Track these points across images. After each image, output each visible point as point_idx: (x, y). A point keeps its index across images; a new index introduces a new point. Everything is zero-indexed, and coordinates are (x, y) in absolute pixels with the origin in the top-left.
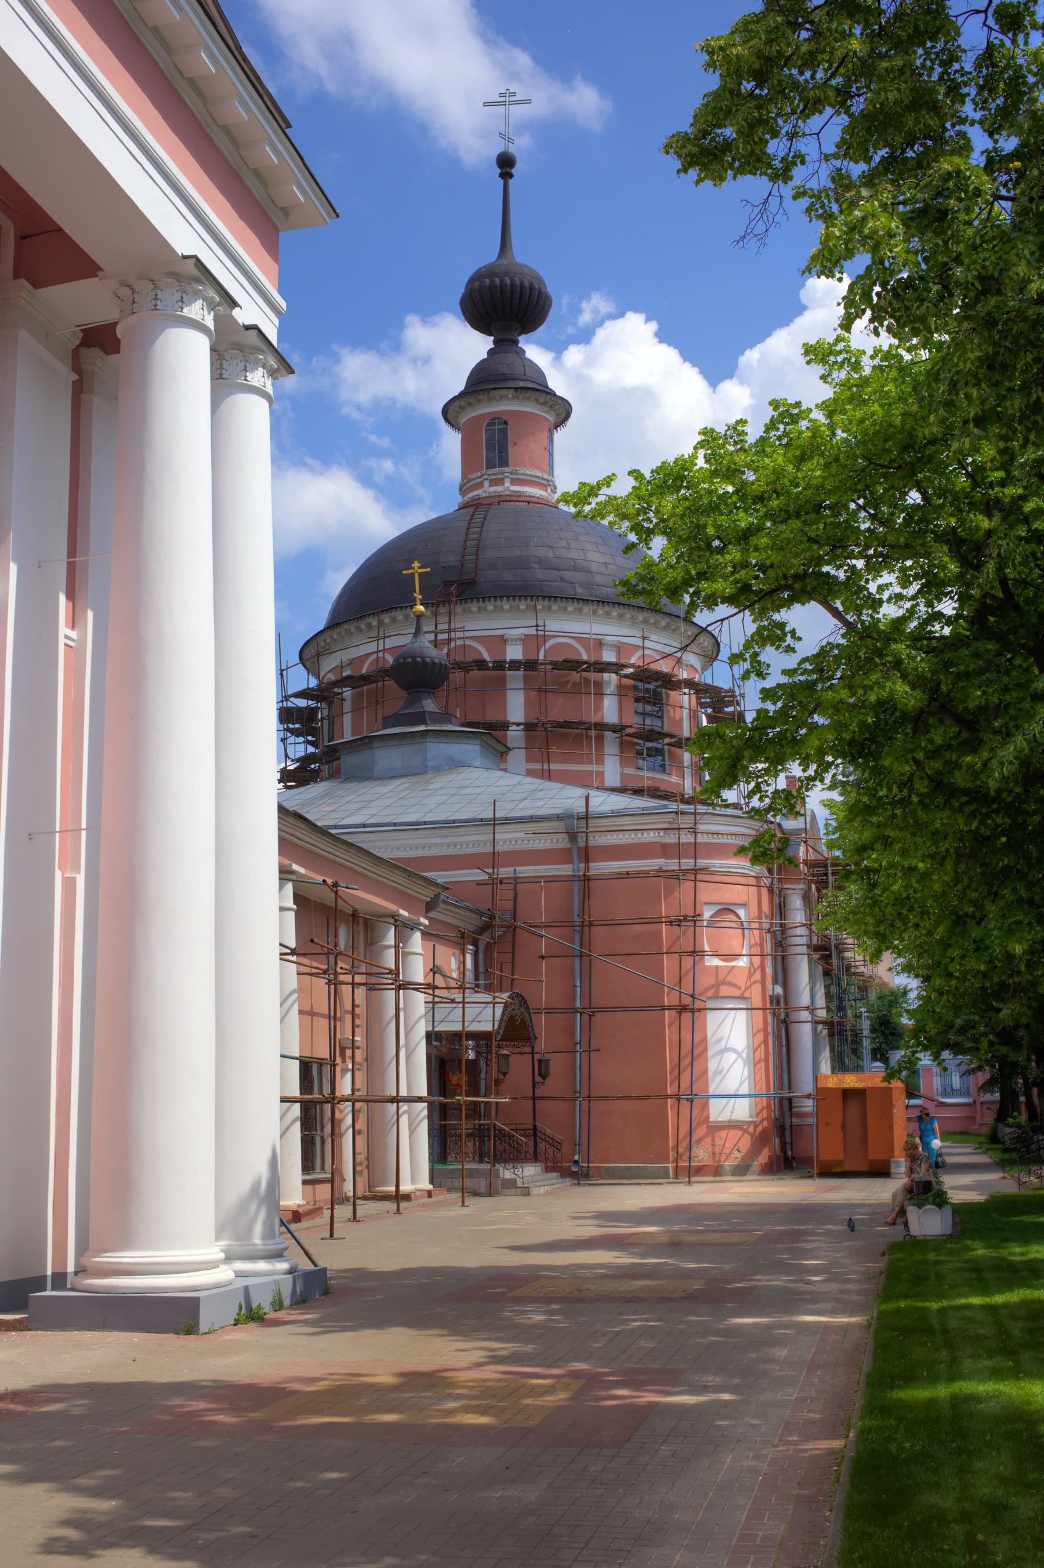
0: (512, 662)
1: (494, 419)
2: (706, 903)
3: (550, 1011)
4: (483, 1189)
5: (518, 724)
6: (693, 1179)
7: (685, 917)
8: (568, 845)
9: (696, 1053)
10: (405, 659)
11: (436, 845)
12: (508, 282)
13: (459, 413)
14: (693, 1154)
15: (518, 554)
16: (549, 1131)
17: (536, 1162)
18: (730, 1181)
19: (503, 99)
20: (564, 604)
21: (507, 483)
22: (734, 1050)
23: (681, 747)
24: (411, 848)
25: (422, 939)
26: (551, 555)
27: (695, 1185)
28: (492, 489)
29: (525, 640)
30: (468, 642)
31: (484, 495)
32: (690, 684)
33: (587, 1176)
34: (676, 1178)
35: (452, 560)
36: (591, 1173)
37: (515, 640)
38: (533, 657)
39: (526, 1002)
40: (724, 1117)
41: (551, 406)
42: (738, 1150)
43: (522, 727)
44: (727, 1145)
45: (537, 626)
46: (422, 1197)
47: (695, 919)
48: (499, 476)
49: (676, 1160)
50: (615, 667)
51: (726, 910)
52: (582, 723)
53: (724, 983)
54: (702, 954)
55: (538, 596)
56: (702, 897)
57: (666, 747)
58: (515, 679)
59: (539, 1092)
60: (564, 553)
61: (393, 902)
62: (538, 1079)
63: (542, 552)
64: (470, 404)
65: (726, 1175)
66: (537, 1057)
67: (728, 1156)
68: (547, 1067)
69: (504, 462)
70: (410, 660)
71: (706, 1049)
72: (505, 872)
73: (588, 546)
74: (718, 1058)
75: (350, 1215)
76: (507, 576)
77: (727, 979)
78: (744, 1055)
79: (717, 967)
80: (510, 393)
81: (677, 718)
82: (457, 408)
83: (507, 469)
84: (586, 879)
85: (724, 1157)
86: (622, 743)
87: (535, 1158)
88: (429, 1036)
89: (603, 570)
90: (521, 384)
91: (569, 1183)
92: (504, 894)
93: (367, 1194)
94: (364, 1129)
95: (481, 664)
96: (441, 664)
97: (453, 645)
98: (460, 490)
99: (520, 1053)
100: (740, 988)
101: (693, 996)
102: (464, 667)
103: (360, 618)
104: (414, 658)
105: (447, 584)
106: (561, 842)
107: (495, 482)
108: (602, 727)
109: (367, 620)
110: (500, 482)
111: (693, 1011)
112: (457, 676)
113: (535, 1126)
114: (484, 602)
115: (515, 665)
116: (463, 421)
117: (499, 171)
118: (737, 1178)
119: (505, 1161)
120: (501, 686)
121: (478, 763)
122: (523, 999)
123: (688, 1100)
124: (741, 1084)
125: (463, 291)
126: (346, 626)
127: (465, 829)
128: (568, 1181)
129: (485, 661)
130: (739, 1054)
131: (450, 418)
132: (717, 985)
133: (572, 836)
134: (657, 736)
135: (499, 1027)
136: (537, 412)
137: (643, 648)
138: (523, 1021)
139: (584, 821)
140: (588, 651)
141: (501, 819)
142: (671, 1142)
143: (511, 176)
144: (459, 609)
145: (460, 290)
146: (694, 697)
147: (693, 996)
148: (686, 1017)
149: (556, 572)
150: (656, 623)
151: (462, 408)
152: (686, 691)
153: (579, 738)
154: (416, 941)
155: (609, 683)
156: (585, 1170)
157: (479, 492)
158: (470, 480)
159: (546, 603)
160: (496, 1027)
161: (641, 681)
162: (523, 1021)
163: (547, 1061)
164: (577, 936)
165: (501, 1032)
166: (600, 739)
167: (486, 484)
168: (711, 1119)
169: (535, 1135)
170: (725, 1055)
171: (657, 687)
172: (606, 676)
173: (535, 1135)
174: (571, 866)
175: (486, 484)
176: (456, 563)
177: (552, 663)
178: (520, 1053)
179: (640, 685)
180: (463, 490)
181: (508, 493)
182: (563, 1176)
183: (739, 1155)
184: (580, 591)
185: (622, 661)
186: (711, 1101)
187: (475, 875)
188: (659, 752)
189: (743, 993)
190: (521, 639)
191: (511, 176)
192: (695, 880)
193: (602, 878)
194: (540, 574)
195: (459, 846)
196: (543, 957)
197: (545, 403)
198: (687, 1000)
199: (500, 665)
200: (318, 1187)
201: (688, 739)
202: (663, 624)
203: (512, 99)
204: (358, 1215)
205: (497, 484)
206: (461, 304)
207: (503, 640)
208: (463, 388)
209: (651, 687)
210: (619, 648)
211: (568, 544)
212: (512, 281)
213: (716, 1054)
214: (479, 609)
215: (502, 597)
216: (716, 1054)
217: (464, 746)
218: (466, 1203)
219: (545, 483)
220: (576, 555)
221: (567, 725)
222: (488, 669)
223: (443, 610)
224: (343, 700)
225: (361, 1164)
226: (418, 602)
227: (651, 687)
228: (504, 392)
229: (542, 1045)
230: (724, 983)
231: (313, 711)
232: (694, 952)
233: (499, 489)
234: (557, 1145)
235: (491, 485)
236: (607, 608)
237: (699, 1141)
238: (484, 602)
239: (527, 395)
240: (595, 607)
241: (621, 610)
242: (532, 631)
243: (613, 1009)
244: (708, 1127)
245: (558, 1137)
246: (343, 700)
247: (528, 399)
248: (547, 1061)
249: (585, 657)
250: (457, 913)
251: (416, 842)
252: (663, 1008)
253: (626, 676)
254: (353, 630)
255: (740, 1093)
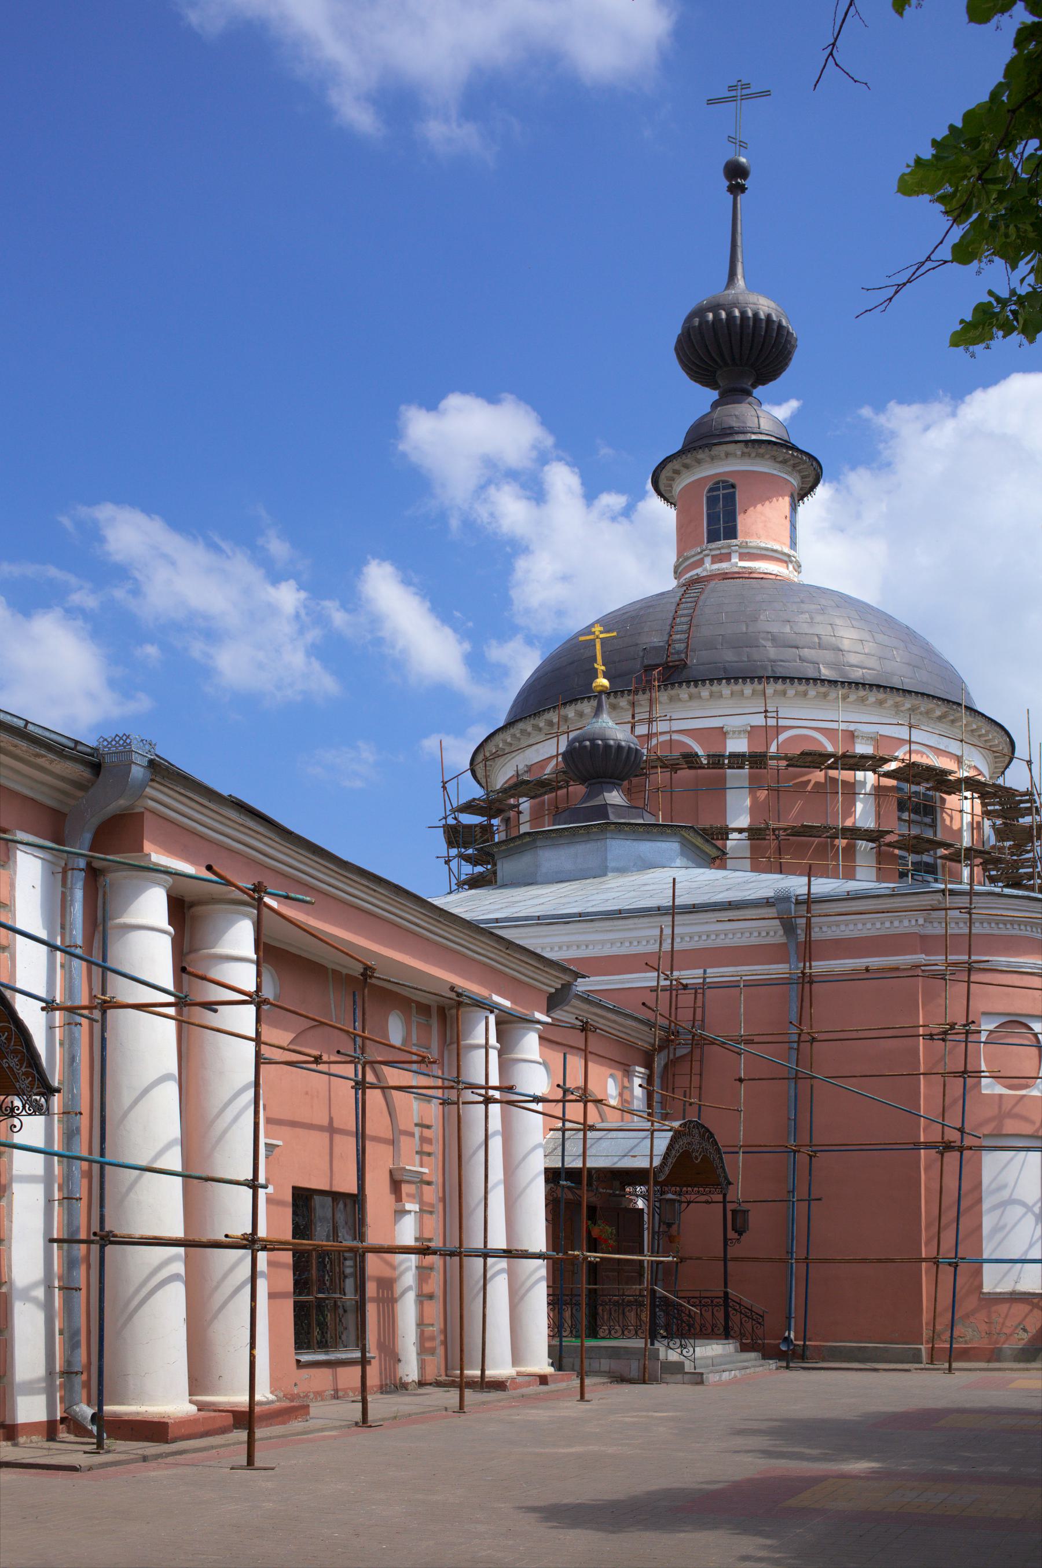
0: (733, 756)
1: (718, 483)
2: (984, 1014)
3: (751, 1150)
4: (634, 1374)
5: (740, 831)
6: (955, 1365)
7: (952, 1026)
8: (784, 940)
9: (964, 1204)
10: (580, 742)
11: (594, 943)
12: (737, 313)
13: (673, 479)
14: (956, 1333)
15: (744, 630)
16: (746, 1301)
17: (727, 1338)
18: (1012, 1370)
19: (733, 93)
20: (802, 688)
21: (735, 559)
22: (1024, 1204)
23: (960, 862)
24: (560, 948)
25: (540, 1044)
26: (787, 629)
27: (957, 1373)
28: (716, 566)
29: (752, 732)
30: (675, 737)
31: (705, 574)
32: (971, 784)
33: (803, 1358)
34: (932, 1363)
35: (657, 640)
36: (808, 1353)
37: (740, 732)
38: (760, 749)
39: (712, 1135)
40: (1004, 1288)
41: (794, 466)
42: (1024, 1330)
43: (746, 834)
44: (1008, 1323)
45: (766, 711)
46: (528, 1384)
47: (969, 1031)
48: (723, 551)
49: (932, 1340)
50: (873, 763)
51: (1016, 1023)
52: (827, 828)
53: (1010, 1115)
54: (978, 1074)
55: (768, 678)
56: (978, 1005)
57: (939, 861)
58: (736, 777)
59: (733, 1251)
60: (805, 628)
61: (482, 983)
62: (731, 1234)
63: (775, 628)
64: (686, 467)
65: (1005, 1360)
66: (730, 1207)
67: (1008, 1336)
68: (745, 1222)
69: (731, 533)
70: (588, 743)
71: (979, 1201)
72: (690, 975)
73: (838, 622)
74: (998, 1212)
75: (358, 1416)
76: (729, 656)
77: (1016, 1110)
78: (1037, 1210)
79: (1001, 1096)
80: (737, 449)
81: (955, 827)
82: (670, 474)
83: (734, 542)
84: (807, 980)
85: (1003, 1337)
86: (879, 854)
87: (726, 1334)
88: (552, 1176)
89: (859, 648)
90: (754, 437)
91: (773, 1366)
92: (686, 999)
93: (443, 1378)
94: (439, 1293)
95: (690, 760)
96: (630, 748)
97: (654, 742)
98: (675, 572)
99: (707, 1202)
100: (1033, 1123)
101: (961, 1130)
102: (672, 766)
103: (537, 714)
104: (592, 741)
105: (649, 669)
106: (778, 936)
107: (717, 559)
108: (854, 833)
109: (547, 716)
110: (727, 557)
111: (961, 1149)
112: (660, 776)
113: (726, 1294)
114: (696, 686)
115: (737, 760)
116: (678, 490)
117: (727, 183)
118: (1022, 1365)
119: (670, 1336)
120: (720, 788)
121: (679, 862)
122: (708, 1130)
123: (950, 1264)
124: (1031, 1246)
125: (679, 331)
126: (521, 725)
127: (636, 920)
128: (772, 1364)
129: (697, 755)
130: (1029, 1209)
131: (662, 488)
132: (1001, 1117)
133: (788, 926)
134: (927, 846)
135: (664, 1163)
136: (775, 472)
137: (910, 742)
138: (705, 1159)
139: (804, 907)
140: (835, 744)
141: (685, 907)
142: (926, 1317)
143: (742, 189)
144: (663, 696)
145: (676, 330)
146: (977, 802)
147: (961, 1130)
148: (952, 1157)
149: (794, 650)
150: (927, 713)
151: (677, 472)
152: (968, 794)
153: (822, 852)
154: (530, 1044)
155: (864, 783)
156: (799, 1350)
157: (698, 571)
158: (687, 559)
159: (780, 686)
160: (657, 1162)
161: (907, 781)
162: (705, 1159)
163: (745, 1212)
164: (794, 1053)
165: (667, 1170)
166: (850, 852)
167: (708, 560)
168: (985, 1290)
169: (726, 1305)
170: (1009, 1208)
171: (928, 789)
172: (860, 775)
173: (726, 1305)
174: (787, 966)
175: (708, 560)
176: (661, 644)
177: (786, 758)
178: (707, 1202)
179: (906, 786)
180: (678, 572)
181: (736, 570)
182: (765, 1357)
183: (1025, 1336)
184: (826, 673)
185: (881, 753)
186: (986, 1266)
187: (648, 979)
188: (931, 869)
189: (1037, 1131)
190: (745, 731)
191: (742, 189)
192: (969, 982)
193: (830, 978)
194: (772, 652)
195: (627, 944)
196: (741, 1080)
197: (784, 462)
198: (953, 1136)
199: (717, 761)
200: (341, 1371)
201: (968, 850)
202: (938, 713)
203: (745, 92)
204: (370, 1417)
205: (721, 561)
206: (676, 349)
207: (721, 733)
208: (680, 448)
209: (921, 789)
210: (877, 740)
211: (812, 618)
212: (743, 313)
213: (995, 1207)
214: (691, 697)
215: (720, 680)
216: (995, 1207)
217: (659, 844)
218: (587, 1396)
219: (786, 558)
220: (819, 630)
221: (806, 831)
222: (702, 767)
223: (642, 698)
224: (520, 813)
225: (432, 1338)
226: (600, 674)
227: (921, 789)
228: (731, 448)
229: (738, 1192)
230: (1010, 1115)
231: (486, 830)
232: (965, 1072)
233: (724, 566)
234: (758, 1319)
235: (713, 562)
236: (862, 693)
237: (967, 1316)
238: (696, 686)
239: (761, 451)
240: (845, 691)
241: (881, 696)
242: (759, 720)
243: (844, 1148)
244: (980, 1300)
245: (758, 1308)
246: (520, 813)
247: (762, 456)
248: (745, 1212)
249: (830, 749)
250: (614, 1022)
251: (566, 939)
252: (917, 1146)
253: (888, 775)
254: (529, 729)
255: (1029, 1257)
